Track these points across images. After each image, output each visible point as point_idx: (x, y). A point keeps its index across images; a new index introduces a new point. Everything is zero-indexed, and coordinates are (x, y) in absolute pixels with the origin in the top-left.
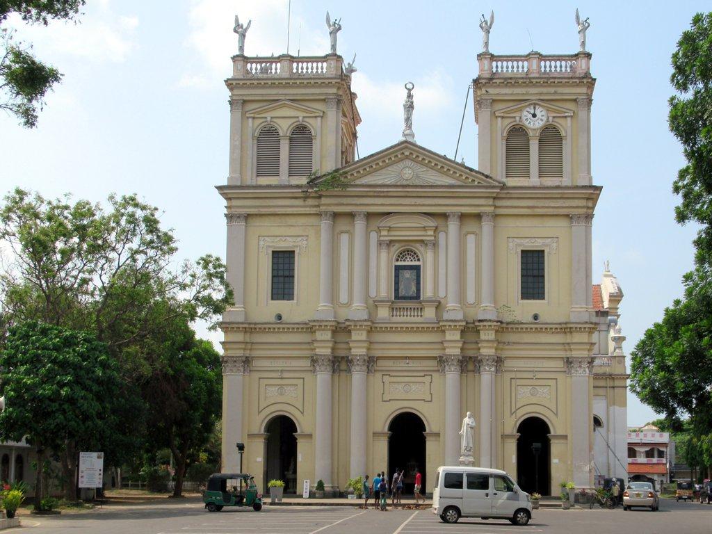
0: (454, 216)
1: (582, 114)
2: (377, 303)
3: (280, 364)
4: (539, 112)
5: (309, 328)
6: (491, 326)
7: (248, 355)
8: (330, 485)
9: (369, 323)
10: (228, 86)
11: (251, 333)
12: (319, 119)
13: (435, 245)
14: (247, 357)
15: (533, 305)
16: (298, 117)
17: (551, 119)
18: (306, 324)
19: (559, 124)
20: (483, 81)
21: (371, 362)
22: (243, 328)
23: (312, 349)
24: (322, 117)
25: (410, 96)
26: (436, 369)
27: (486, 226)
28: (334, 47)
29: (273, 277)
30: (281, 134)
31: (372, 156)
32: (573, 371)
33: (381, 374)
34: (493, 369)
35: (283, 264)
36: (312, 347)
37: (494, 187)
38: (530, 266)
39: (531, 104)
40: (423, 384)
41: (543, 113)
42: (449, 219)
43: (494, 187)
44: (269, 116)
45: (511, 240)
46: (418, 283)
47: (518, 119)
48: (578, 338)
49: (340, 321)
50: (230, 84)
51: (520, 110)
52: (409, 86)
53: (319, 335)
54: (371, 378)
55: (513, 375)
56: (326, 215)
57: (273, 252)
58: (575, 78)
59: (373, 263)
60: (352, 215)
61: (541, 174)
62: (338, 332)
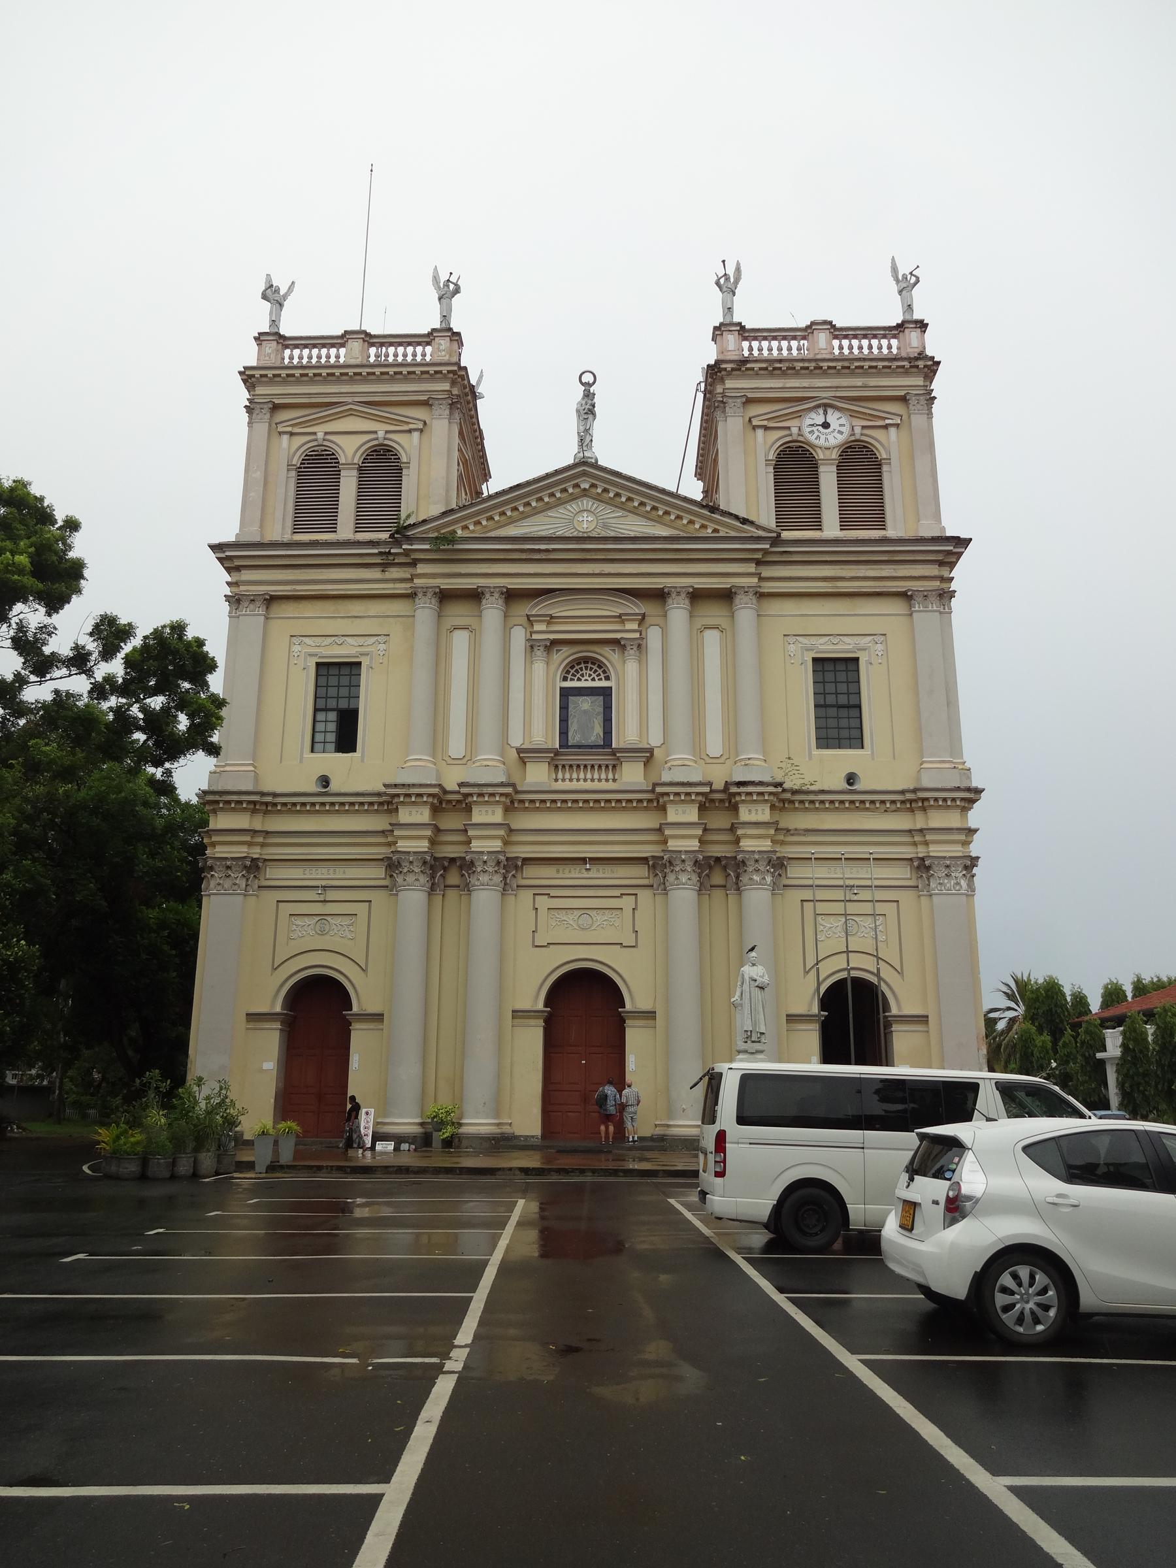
0: (679, 593)
1: (917, 420)
2: (525, 755)
3: (321, 874)
4: (833, 418)
5: (388, 801)
6: (762, 794)
7: (255, 856)
8: (418, 1120)
9: (509, 790)
10: (245, 381)
11: (266, 812)
12: (416, 435)
13: (640, 646)
14: (253, 860)
15: (843, 759)
16: (376, 432)
17: (858, 430)
18: (379, 794)
19: (876, 440)
20: (729, 366)
21: (511, 867)
22: (249, 802)
23: (389, 844)
24: (421, 431)
25: (588, 395)
26: (646, 882)
27: (745, 612)
28: (445, 318)
29: (316, 710)
30: (342, 460)
31: (518, 487)
32: (933, 885)
33: (531, 892)
34: (769, 879)
35: (337, 685)
36: (390, 839)
37: (759, 539)
38: (830, 688)
39: (818, 406)
40: (618, 912)
41: (843, 421)
42: (670, 601)
43: (759, 539)
44: (320, 430)
45: (791, 639)
46: (607, 720)
47: (795, 430)
48: (938, 819)
49: (448, 788)
50: (249, 378)
51: (798, 415)
52: (588, 378)
53: (406, 815)
54: (511, 899)
55: (807, 894)
56: (425, 594)
57: (318, 664)
58: (902, 359)
59: (517, 683)
60: (475, 596)
61: (844, 524)
62: (444, 810)
